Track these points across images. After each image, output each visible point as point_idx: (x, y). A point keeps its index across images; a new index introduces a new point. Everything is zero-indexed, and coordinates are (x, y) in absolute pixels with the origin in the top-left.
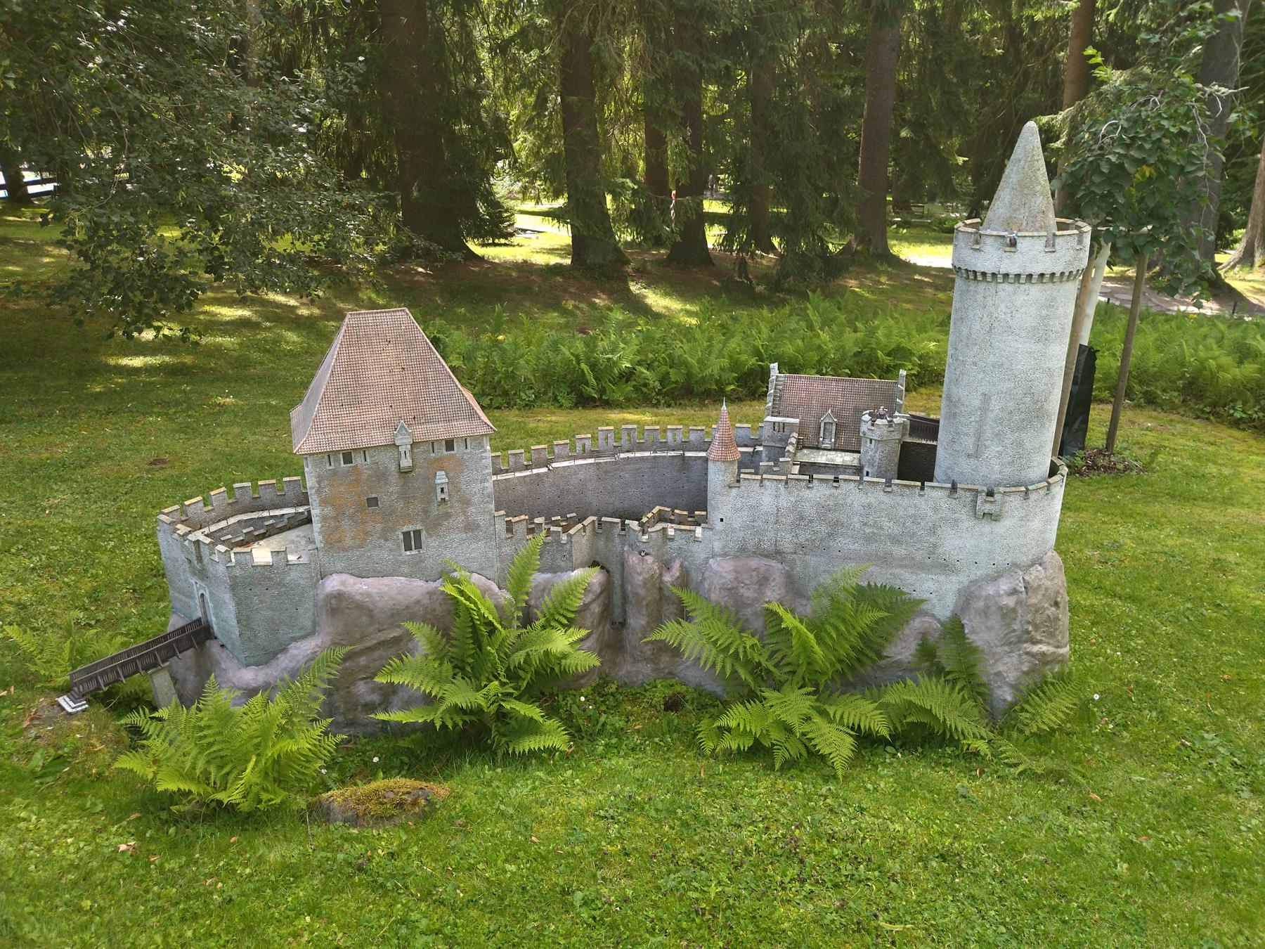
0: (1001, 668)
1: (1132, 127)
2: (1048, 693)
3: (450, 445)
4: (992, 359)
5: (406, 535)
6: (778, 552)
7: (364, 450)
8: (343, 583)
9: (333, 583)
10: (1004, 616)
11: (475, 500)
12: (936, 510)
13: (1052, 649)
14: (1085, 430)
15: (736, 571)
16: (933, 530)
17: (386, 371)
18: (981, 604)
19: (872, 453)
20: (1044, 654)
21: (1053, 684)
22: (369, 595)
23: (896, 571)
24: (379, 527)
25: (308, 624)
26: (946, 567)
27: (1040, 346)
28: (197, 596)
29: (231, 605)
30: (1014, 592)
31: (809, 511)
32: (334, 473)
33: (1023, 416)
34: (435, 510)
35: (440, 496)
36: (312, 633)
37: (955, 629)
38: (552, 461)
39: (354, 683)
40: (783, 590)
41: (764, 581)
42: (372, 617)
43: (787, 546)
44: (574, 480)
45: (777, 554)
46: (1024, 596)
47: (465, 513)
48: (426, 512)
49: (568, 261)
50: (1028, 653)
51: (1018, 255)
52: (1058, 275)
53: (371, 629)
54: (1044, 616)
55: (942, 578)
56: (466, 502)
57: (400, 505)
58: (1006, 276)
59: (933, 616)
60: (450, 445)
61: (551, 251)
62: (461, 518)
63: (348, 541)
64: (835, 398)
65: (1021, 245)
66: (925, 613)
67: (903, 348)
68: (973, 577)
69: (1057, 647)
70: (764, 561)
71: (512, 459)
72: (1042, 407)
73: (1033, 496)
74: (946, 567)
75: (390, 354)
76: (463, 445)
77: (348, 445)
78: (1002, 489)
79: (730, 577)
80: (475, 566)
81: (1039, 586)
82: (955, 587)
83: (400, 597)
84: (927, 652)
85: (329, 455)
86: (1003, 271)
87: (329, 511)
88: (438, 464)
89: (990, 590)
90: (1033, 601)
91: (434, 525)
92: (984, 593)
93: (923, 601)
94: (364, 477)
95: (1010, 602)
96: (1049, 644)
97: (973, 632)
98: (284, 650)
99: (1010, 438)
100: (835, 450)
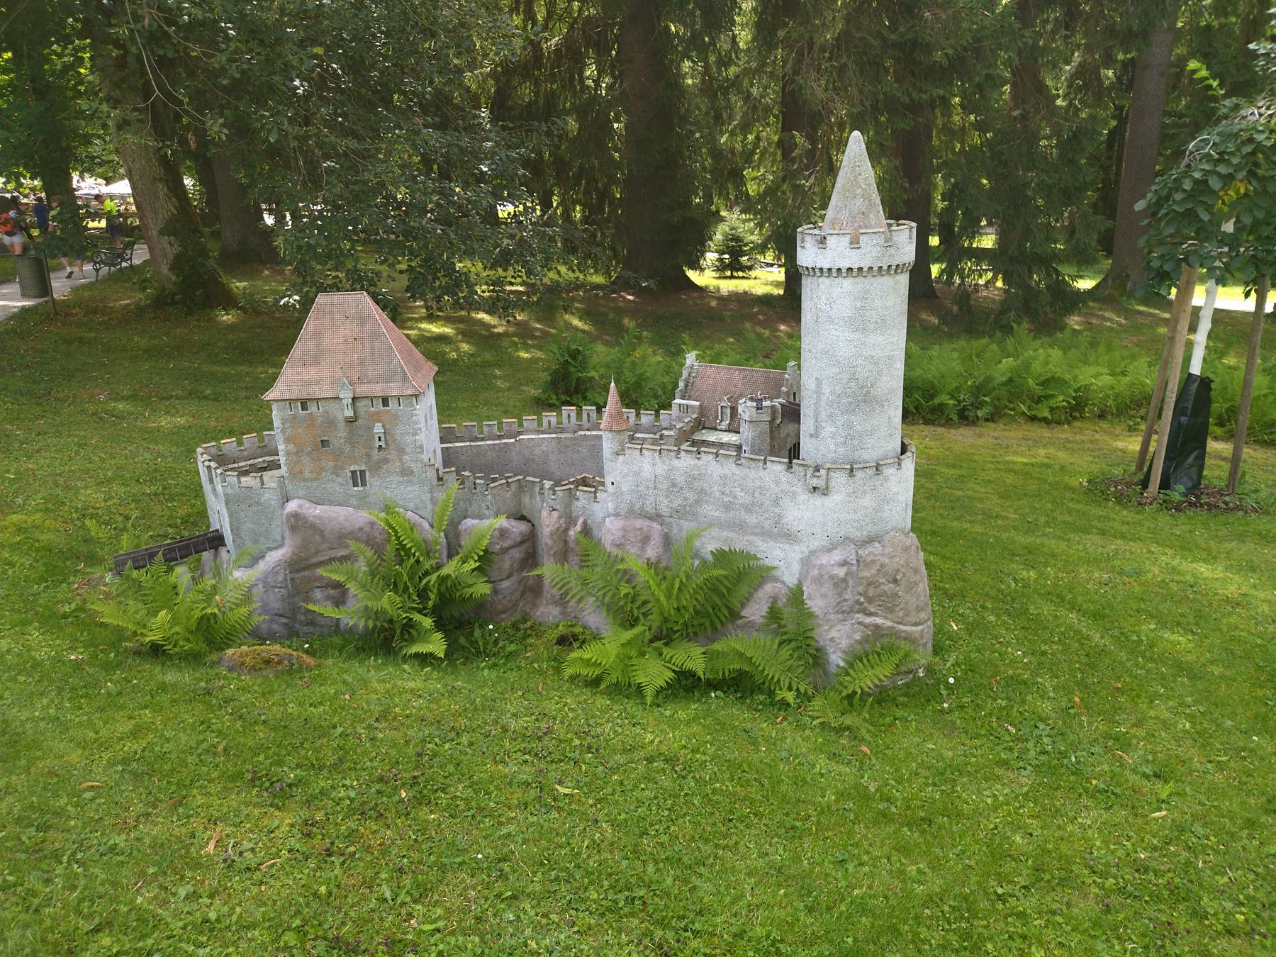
0: (834, 634)
1: (1222, 141)
2: (872, 661)
3: (385, 401)
4: (820, 346)
5: (353, 473)
6: (658, 515)
7: (317, 400)
9: (292, 506)
10: (836, 585)
11: (409, 449)
12: (777, 483)
13: (889, 623)
14: (1201, 468)
15: (624, 530)
16: (776, 502)
17: (341, 341)
18: (816, 572)
19: (747, 434)
20: (877, 626)
21: (879, 654)
22: (320, 518)
23: (750, 538)
24: (331, 464)
25: (279, 538)
26: (789, 537)
27: (858, 335)
30: (844, 563)
31: (680, 480)
32: (294, 417)
33: (850, 399)
34: (376, 455)
35: (378, 444)
36: (281, 546)
37: (796, 596)
38: (520, 433)
39: (311, 589)
40: (661, 550)
41: (646, 540)
42: (323, 536)
43: (665, 511)
44: (538, 451)
45: (657, 517)
47: (401, 460)
48: (368, 456)
49: (781, 292)
50: (860, 623)
51: (828, 251)
52: (865, 269)
53: (324, 546)
55: (787, 547)
56: (401, 451)
57: (347, 448)
58: (839, 270)
59: (783, 582)
61: (772, 283)
62: (398, 464)
63: (307, 474)
64: (736, 386)
65: (831, 241)
66: (776, 580)
67: (1059, 378)
68: (812, 548)
70: (647, 523)
71: (485, 429)
72: (869, 392)
73: (859, 474)
74: (789, 537)
75: (347, 328)
76: (396, 402)
77: (304, 396)
79: (619, 534)
80: (411, 505)
81: (873, 562)
82: (799, 556)
83: (346, 524)
84: (774, 614)
85: (291, 401)
86: (819, 266)
87: (291, 447)
88: (377, 417)
89: (824, 559)
90: (866, 574)
91: (377, 467)
93: (774, 568)
94: (318, 423)
95: (841, 572)
97: (809, 598)
98: (263, 557)
99: (840, 420)
100: (729, 431)
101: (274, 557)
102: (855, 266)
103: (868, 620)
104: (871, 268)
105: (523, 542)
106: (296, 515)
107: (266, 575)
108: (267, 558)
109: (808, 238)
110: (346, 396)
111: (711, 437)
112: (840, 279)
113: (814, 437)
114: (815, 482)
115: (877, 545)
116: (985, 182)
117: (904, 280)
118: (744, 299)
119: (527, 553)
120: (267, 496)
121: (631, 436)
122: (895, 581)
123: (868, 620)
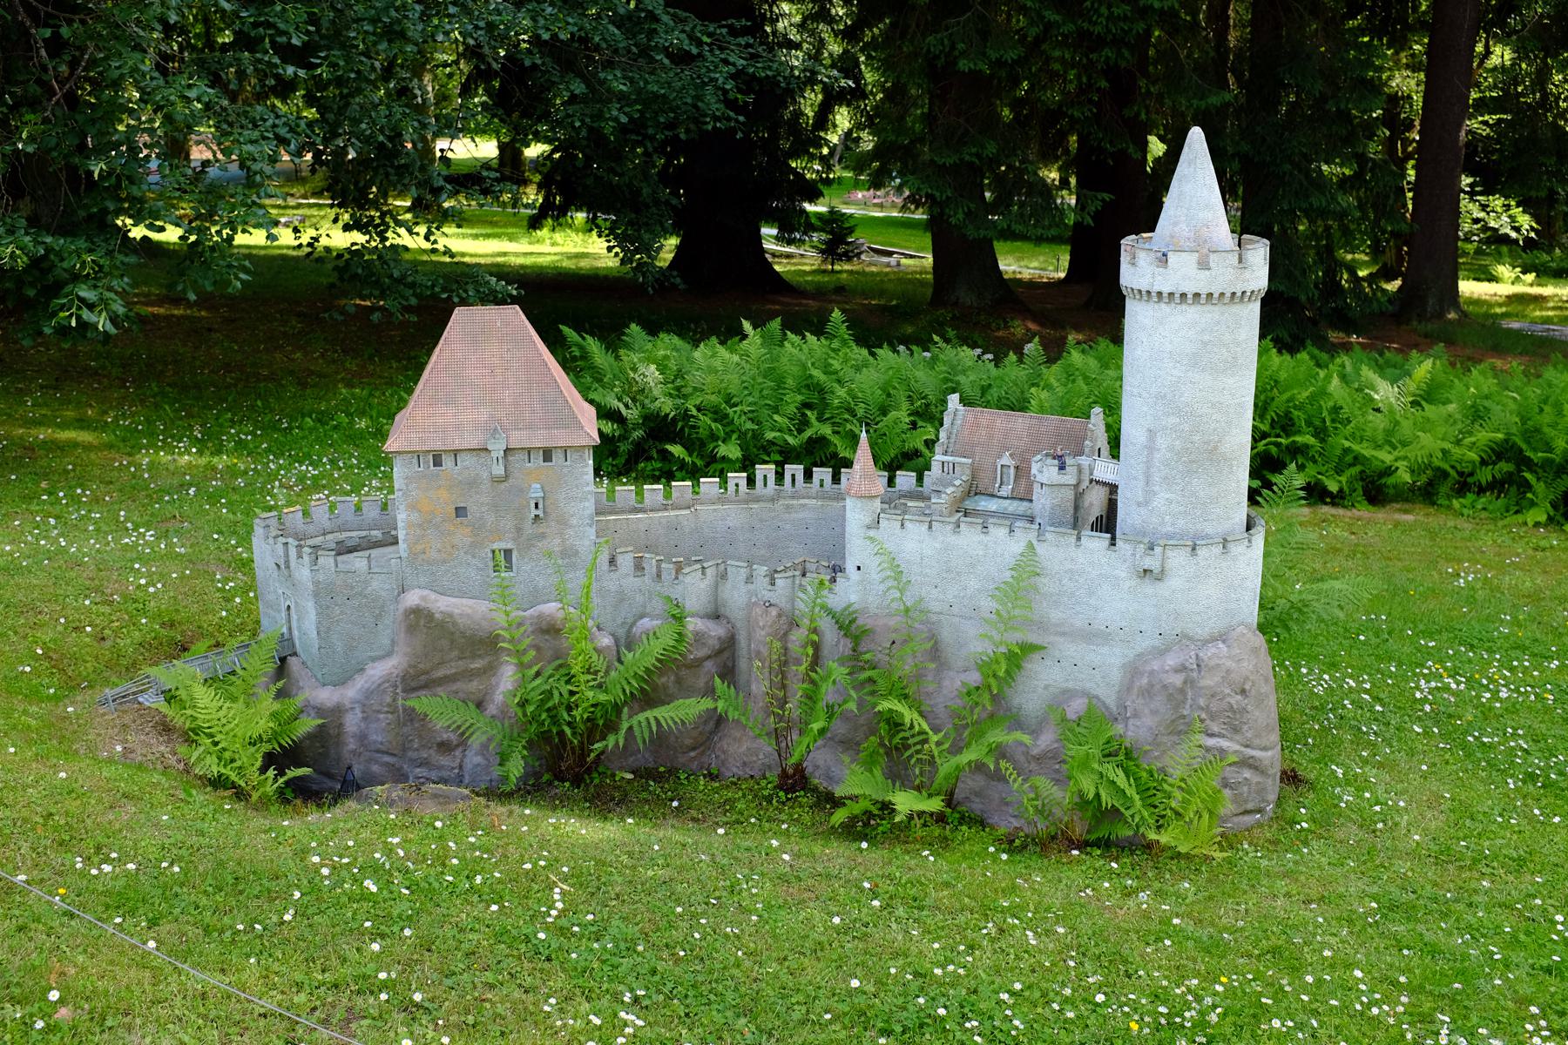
3: (547, 455)
8: (423, 598)
9: (413, 598)
10: (1170, 697)
18: (1145, 681)
25: (387, 642)
28: (284, 608)
29: (312, 616)
30: (1183, 668)
34: (529, 529)
35: (534, 512)
36: (389, 654)
46: (1195, 674)
48: (519, 530)
54: (1224, 705)
56: (563, 522)
58: (1183, 295)
60: (547, 455)
69: (1247, 746)
73: (1201, 552)
76: (562, 456)
77: (438, 446)
78: (1162, 542)
83: (484, 623)
85: (418, 455)
86: (1156, 288)
87: (415, 517)
89: (1155, 665)
92: (1148, 668)
95: (1177, 680)
96: (1231, 739)
101: (380, 670)
102: (1204, 292)
103: (1211, 742)
104: (1222, 294)
105: (720, 652)
106: (416, 612)
107: (368, 694)
108: (370, 672)
109: (1141, 255)
110: (497, 448)
111: (992, 505)
112: (1184, 307)
113: (1132, 502)
114: (1149, 562)
115: (1221, 645)
116: (1006, 112)
117: (1256, 307)
118: (159, 244)
119: (725, 665)
120: (375, 584)
121: (893, 502)
122: (1243, 692)
123: (1211, 742)
